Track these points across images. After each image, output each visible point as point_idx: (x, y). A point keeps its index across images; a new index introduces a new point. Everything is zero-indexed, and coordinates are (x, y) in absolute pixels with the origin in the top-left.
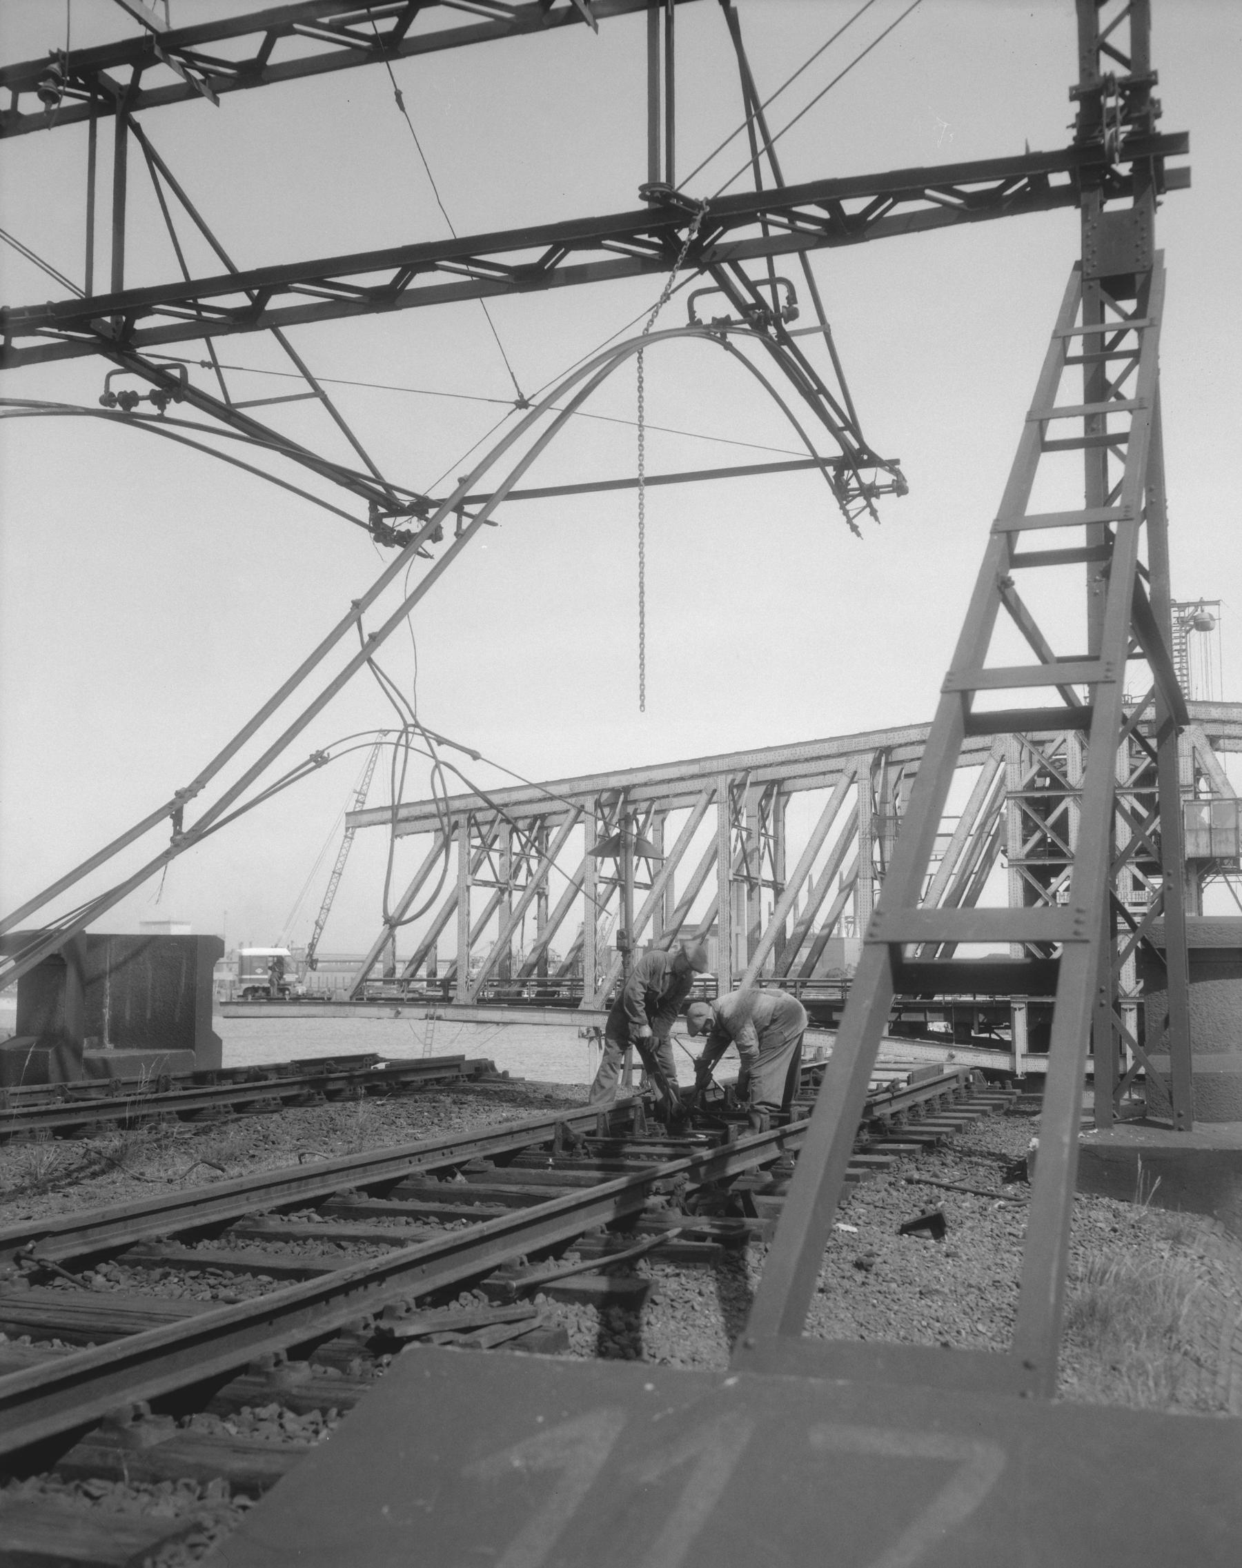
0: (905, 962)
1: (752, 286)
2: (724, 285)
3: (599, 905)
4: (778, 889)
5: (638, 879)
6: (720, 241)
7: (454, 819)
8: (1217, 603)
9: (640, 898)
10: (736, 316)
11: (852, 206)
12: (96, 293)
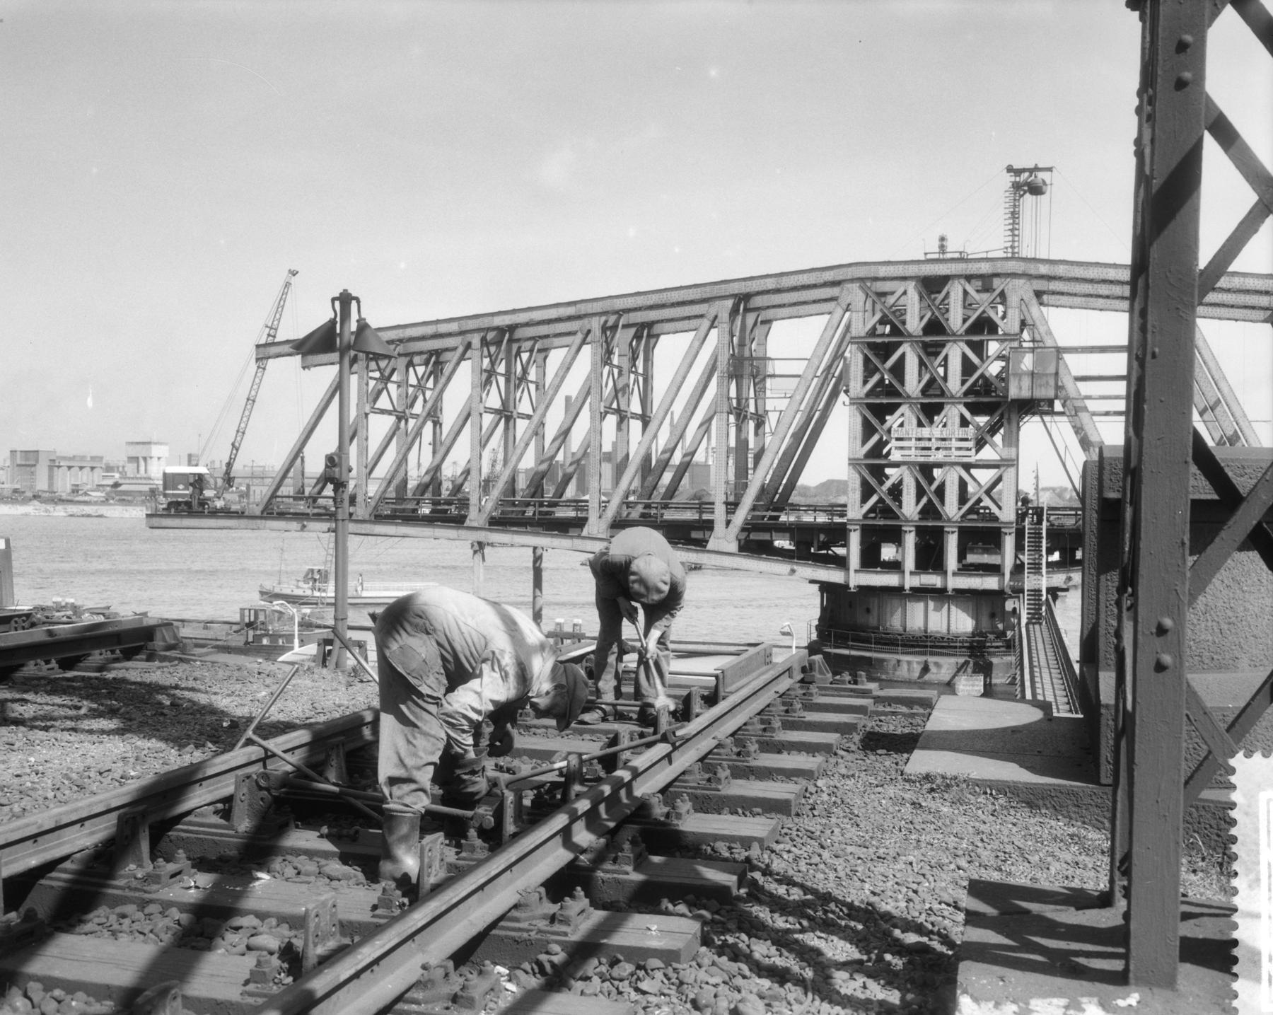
8: (1050, 169)
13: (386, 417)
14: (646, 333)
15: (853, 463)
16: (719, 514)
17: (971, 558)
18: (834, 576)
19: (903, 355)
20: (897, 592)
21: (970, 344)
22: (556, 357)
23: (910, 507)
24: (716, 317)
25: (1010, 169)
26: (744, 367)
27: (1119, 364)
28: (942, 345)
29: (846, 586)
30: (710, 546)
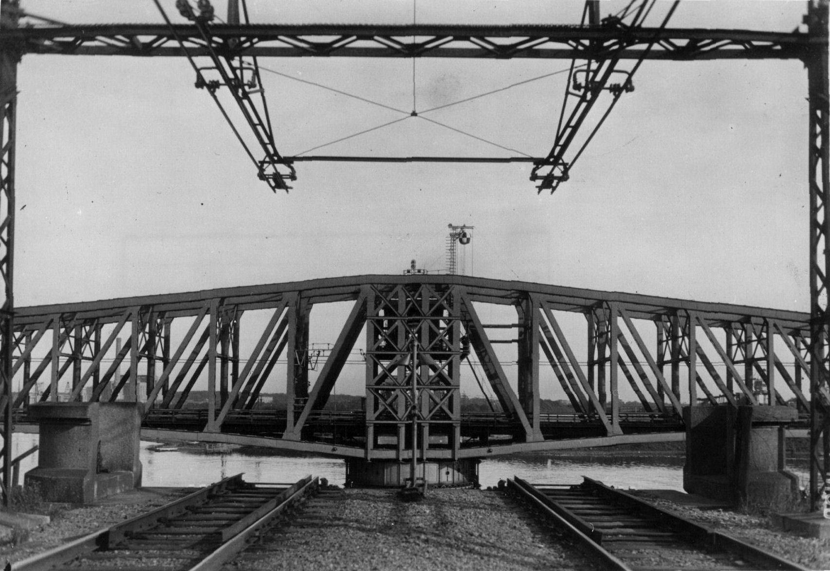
0: (36, 428)
1: (233, 70)
2: (219, 67)
3: (137, 359)
4: (165, 359)
5: (84, 355)
6: (165, 45)
7: (51, 317)
8: (472, 228)
9: (85, 366)
10: (222, 81)
11: (144, 39)
12: (624, 21)
13: (513, 329)
14: (237, 311)
15: (368, 387)
16: (290, 417)
17: (381, 440)
18: (359, 453)
19: (397, 327)
20: (396, 461)
21: (433, 321)
22: (107, 330)
23: (402, 412)
24: (131, 314)
25: (450, 226)
26: (227, 333)
27: (514, 333)
28: (418, 321)
29: (366, 459)
30: (284, 437)
